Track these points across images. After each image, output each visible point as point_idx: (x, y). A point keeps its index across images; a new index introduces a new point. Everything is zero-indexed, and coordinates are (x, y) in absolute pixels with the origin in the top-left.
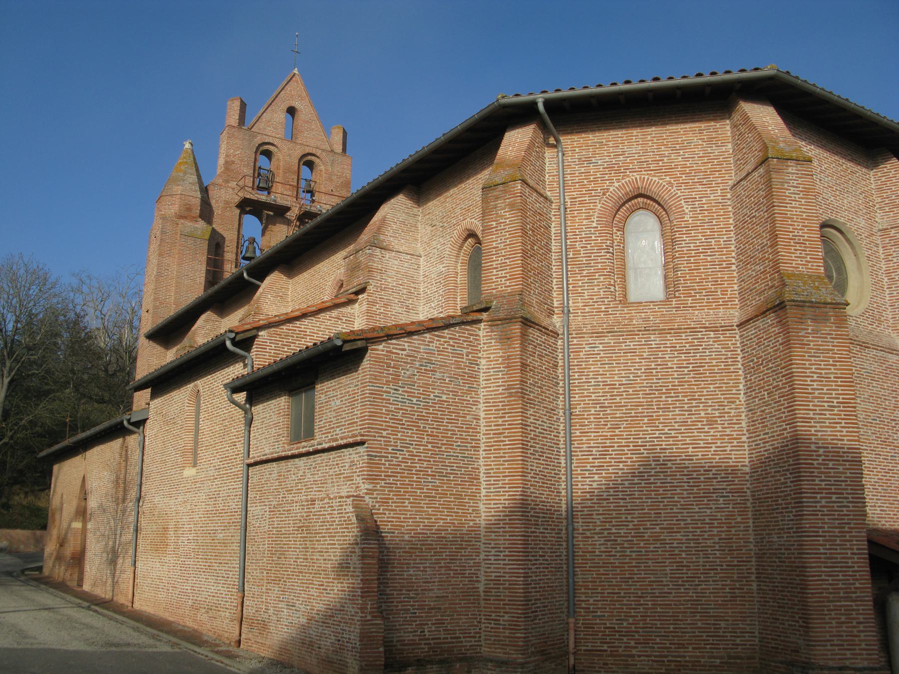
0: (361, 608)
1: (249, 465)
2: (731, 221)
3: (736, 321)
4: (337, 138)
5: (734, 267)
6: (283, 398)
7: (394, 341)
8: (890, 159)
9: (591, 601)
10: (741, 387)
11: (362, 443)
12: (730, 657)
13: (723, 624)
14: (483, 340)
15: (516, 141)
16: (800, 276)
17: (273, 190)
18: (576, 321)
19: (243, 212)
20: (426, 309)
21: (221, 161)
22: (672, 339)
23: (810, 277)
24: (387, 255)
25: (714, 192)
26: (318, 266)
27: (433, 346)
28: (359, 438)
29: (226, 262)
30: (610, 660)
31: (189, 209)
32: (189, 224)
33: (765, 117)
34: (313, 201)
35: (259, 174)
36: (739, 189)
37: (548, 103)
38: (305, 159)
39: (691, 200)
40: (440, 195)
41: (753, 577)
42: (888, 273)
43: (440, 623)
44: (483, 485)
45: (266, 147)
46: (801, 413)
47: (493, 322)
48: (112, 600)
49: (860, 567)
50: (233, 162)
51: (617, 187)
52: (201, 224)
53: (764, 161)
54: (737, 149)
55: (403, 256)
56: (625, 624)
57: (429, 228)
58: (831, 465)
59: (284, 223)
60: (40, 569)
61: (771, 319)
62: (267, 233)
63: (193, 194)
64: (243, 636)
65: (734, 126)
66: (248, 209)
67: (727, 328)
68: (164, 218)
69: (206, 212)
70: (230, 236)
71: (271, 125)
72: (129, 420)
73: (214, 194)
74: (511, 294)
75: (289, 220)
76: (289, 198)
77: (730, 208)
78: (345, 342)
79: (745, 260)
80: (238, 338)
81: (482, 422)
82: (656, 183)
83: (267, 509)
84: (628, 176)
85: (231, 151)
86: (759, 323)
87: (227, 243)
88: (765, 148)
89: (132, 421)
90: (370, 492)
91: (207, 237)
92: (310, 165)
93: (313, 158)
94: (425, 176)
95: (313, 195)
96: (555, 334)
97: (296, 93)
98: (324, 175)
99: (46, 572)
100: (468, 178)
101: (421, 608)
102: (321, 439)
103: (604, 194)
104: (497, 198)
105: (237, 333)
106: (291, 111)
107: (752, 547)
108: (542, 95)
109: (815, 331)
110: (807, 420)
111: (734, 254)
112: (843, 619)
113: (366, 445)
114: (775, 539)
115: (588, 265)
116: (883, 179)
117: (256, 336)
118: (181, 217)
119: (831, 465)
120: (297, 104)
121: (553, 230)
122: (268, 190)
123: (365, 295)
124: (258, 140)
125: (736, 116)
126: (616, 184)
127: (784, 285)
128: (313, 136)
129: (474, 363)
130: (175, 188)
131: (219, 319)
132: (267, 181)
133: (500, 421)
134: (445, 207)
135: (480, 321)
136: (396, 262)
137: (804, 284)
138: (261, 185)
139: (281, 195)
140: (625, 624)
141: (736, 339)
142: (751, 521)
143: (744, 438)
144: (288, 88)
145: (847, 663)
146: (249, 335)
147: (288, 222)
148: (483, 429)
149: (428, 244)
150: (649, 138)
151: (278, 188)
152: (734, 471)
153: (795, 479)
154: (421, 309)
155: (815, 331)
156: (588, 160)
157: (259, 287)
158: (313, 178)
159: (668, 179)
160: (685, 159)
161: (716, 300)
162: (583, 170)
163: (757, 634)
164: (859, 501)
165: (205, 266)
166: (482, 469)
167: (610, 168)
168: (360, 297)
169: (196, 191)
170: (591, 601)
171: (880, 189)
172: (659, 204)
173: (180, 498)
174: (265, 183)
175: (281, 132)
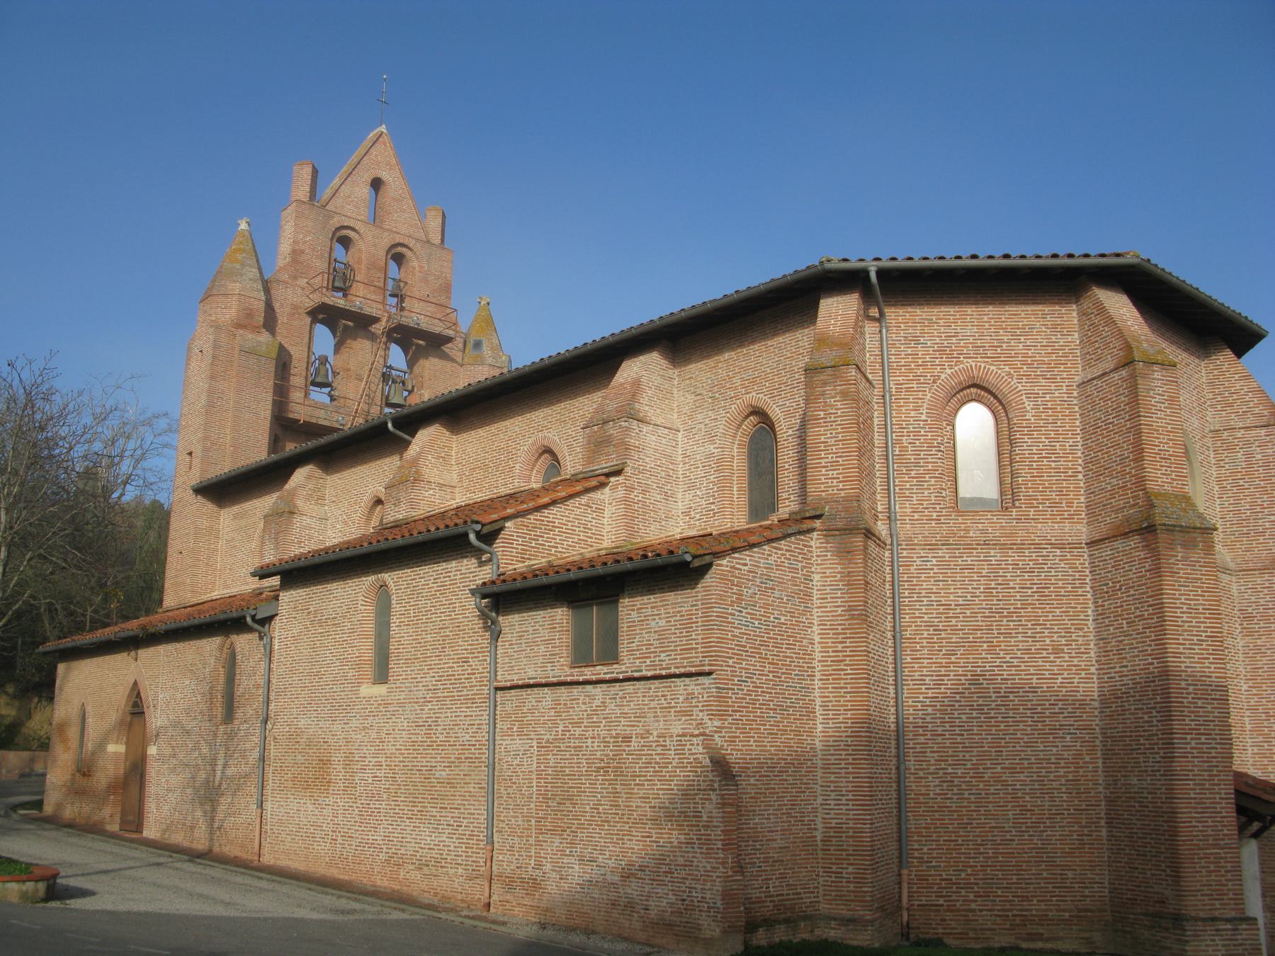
0: (723, 863)
1: (497, 689)
2: (1078, 423)
3: (1084, 538)
4: (434, 223)
5: (1080, 476)
6: (559, 610)
7: (736, 555)
8: (1220, 350)
9: (925, 849)
10: (1090, 612)
11: (709, 674)
12: (1080, 911)
13: (1070, 874)
14: (816, 552)
15: (837, 311)
16: (1166, 496)
17: (353, 291)
18: (904, 529)
19: (315, 320)
20: (689, 496)
21: (285, 248)
22: (1013, 556)
23: (1176, 496)
24: (645, 428)
25: (1059, 388)
26: (504, 423)
27: (772, 560)
28: (707, 668)
29: (292, 390)
30: (949, 916)
31: (250, 315)
32: (250, 336)
33: (1119, 306)
34: (402, 309)
35: (335, 270)
36: (1090, 389)
37: (881, 273)
38: (394, 251)
39: (1032, 396)
40: (708, 357)
41: (1103, 823)
42: (1219, 481)
43: (783, 877)
44: (819, 719)
45: (345, 232)
46: (1171, 648)
47: (829, 532)
48: (211, 851)
49: (1227, 810)
50: (303, 251)
51: (948, 374)
52: (265, 337)
53: (1128, 362)
54: (1086, 341)
55: (662, 431)
56: (963, 875)
57: (691, 398)
58: (1200, 703)
59: (368, 338)
60: (39, 805)
61: (1135, 541)
62: (343, 350)
63: (255, 294)
64: (495, 897)
65: (1082, 314)
66: (321, 316)
67: (1074, 546)
68: (218, 327)
69: (270, 322)
70: (297, 353)
71: (351, 201)
72: (253, 617)
73: (279, 293)
74: (846, 499)
75: (373, 334)
76: (374, 305)
77: (1077, 409)
78: (695, 557)
79: (1095, 468)
80: (486, 530)
81: (817, 647)
82: (995, 372)
83: (535, 744)
84: (962, 362)
85: (294, 234)
86: (1119, 544)
87: (294, 363)
88: (1128, 348)
89: (258, 617)
90: (719, 730)
91: (274, 355)
92: (399, 259)
93: (403, 250)
94: (687, 336)
95: (402, 301)
96: (881, 544)
97: (382, 158)
98: (418, 274)
99: (48, 809)
100: (753, 342)
101: (766, 860)
102: (626, 666)
103: (934, 382)
104: (825, 383)
105: (483, 525)
106: (377, 184)
107: (1101, 789)
108: (875, 263)
109: (1185, 559)
110: (1177, 655)
111: (1080, 461)
112: (1212, 867)
113: (714, 676)
114: (1135, 781)
115: (917, 464)
116: (1216, 372)
117: (502, 529)
118: (239, 326)
119: (1200, 703)
120: (384, 175)
121: (876, 421)
122: (345, 291)
123: (621, 479)
124: (335, 222)
125: (1086, 303)
126: (949, 371)
127: (1152, 506)
128: (404, 220)
129: (808, 579)
130: (231, 286)
131: (324, 476)
132: (345, 280)
133: (840, 647)
134: (716, 374)
135: (813, 530)
136: (654, 438)
137: (1172, 504)
138: (337, 284)
139: (363, 299)
140: (963, 875)
141: (1083, 559)
142: (1100, 761)
143: (1093, 670)
144: (374, 152)
145: (1217, 913)
146: (496, 526)
147: (373, 337)
148: (818, 656)
149: (691, 417)
150: (986, 318)
151: (359, 290)
152: (1083, 704)
153: (1151, 716)
154: (680, 496)
155: (1185, 559)
156: (916, 340)
157: (409, 443)
158: (402, 275)
159: (1007, 368)
160: (1027, 347)
161: (1061, 513)
162: (909, 351)
163: (1106, 885)
164: (1227, 743)
165: (271, 394)
166: (818, 701)
167: (941, 351)
168: (612, 479)
169: (258, 291)
170: (925, 849)
171: (1210, 383)
172: (995, 397)
173: (355, 723)
174: (341, 280)
175: (364, 213)
